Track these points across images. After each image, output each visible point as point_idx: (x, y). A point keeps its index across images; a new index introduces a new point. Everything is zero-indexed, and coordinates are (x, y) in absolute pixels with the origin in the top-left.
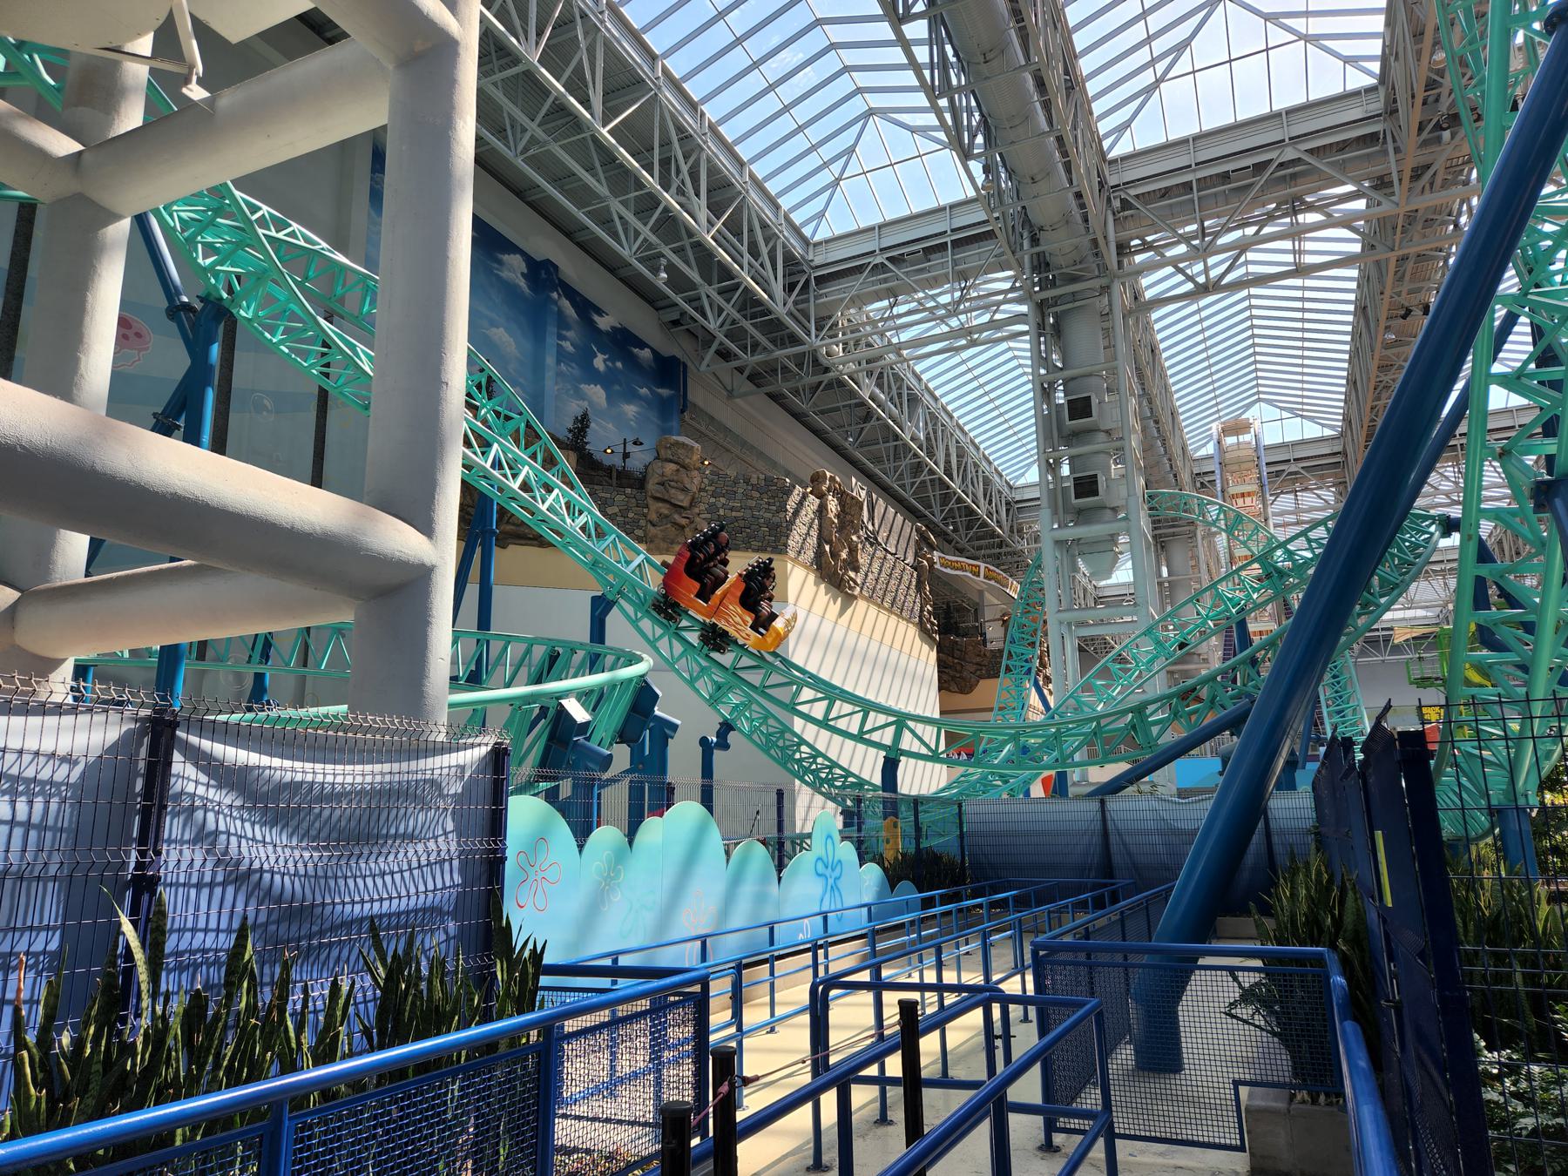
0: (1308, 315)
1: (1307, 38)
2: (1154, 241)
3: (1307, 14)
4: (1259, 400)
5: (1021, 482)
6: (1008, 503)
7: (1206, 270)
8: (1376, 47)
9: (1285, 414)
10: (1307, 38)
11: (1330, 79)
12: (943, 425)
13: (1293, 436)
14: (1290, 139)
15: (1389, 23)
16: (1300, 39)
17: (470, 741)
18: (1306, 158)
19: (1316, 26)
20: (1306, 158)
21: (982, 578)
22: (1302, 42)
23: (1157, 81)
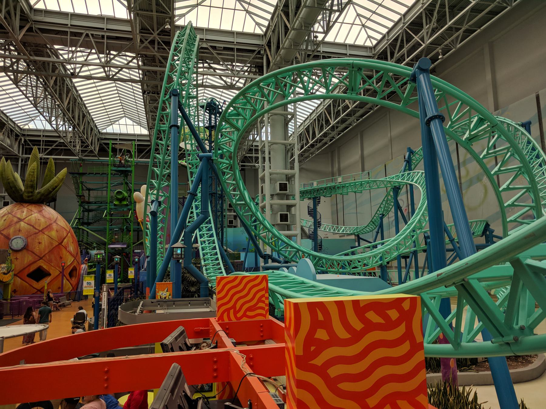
0: (98, 88)
1: (247, 11)
2: (336, 75)
3: (249, 4)
4: (125, 116)
5: (104, 131)
6: (98, 139)
7: (237, 81)
8: (266, 23)
9: (135, 124)
10: (247, 11)
11: (250, 28)
12: (78, 103)
13: (131, 131)
14: (206, 40)
15: (272, 18)
16: (245, 11)
17: (451, 376)
18: (210, 48)
19: (251, 9)
20: (210, 48)
21: (30, 156)
22: (245, 12)
23: (197, 4)
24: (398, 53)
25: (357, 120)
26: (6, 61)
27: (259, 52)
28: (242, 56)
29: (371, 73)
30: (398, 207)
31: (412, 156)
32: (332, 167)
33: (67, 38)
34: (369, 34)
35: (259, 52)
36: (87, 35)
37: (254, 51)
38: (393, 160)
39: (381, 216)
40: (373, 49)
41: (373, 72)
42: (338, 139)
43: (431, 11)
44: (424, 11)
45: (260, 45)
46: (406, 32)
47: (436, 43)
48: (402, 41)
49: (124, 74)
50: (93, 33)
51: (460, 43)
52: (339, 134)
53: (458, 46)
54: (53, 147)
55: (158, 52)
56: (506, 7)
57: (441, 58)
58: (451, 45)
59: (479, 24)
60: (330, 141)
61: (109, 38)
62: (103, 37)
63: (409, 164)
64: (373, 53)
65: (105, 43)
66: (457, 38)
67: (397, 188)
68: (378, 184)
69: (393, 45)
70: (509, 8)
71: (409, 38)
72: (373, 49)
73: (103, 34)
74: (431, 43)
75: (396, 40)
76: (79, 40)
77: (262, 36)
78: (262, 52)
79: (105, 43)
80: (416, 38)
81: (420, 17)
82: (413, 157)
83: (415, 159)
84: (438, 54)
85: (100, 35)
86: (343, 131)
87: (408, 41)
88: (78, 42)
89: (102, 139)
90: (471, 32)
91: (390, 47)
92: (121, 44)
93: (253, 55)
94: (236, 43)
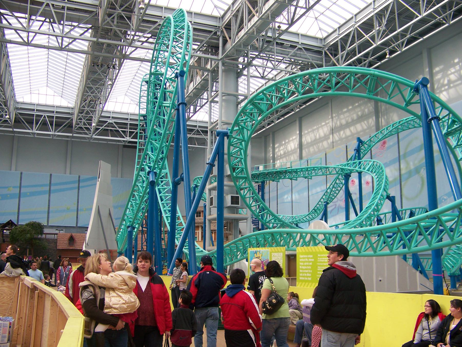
24: (349, 47)
25: (300, 106)
26: (246, 91)
27: (215, 33)
28: (198, 36)
29: (321, 63)
30: (348, 195)
31: (361, 146)
32: (266, 152)
33: (27, 6)
34: (321, 27)
35: (215, 33)
36: (48, 5)
37: (211, 32)
38: (335, 148)
39: (325, 203)
40: (323, 40)
41: (322, 61)
42: (278, 123)
43: (380, 15)
44: (375, 15)
45: (217, 27)
46: (357, 30)
47: (386, 44)
48: (353, 37)
49: (76, 45)
50: (53, 3)
51: (405, 47)
52: (279, 119)
53: (404, 49)
54: (103, 127)
55: (117, 26)
56: (445, 24)
57: (387, 58)
58: (397, 47)
59: (422, 34)
60: (268, 126)
61: (69, 9)
62: (63, 8)
63: (358, 154)
64: (323, 44)
65: (65, 14)
66: (403, 43)
67: (348, 175)
68: (330, 170)
69: (344, 40)
70: (447, 25)
71: (360, 36)
72: (323, 40)
73: (64, 5)
74: (382, 44)
75: (348, 35)
76: (40, 9)
77: (219, 18)
78: (219, 33)
79: (65, 14)
80: (367, 37)
81: (371, 19)
82: (362, 146)
83: (364, 149)
84: (385, 55)
85: (61, 6)
86: (283, 116)
87: (359, 38)
88: (38, 12)
89: (18, 109)
90: (415, 39)
91: (341, 42)
92: (79, 16)
93: (209, 36)
94: (194, 22)
